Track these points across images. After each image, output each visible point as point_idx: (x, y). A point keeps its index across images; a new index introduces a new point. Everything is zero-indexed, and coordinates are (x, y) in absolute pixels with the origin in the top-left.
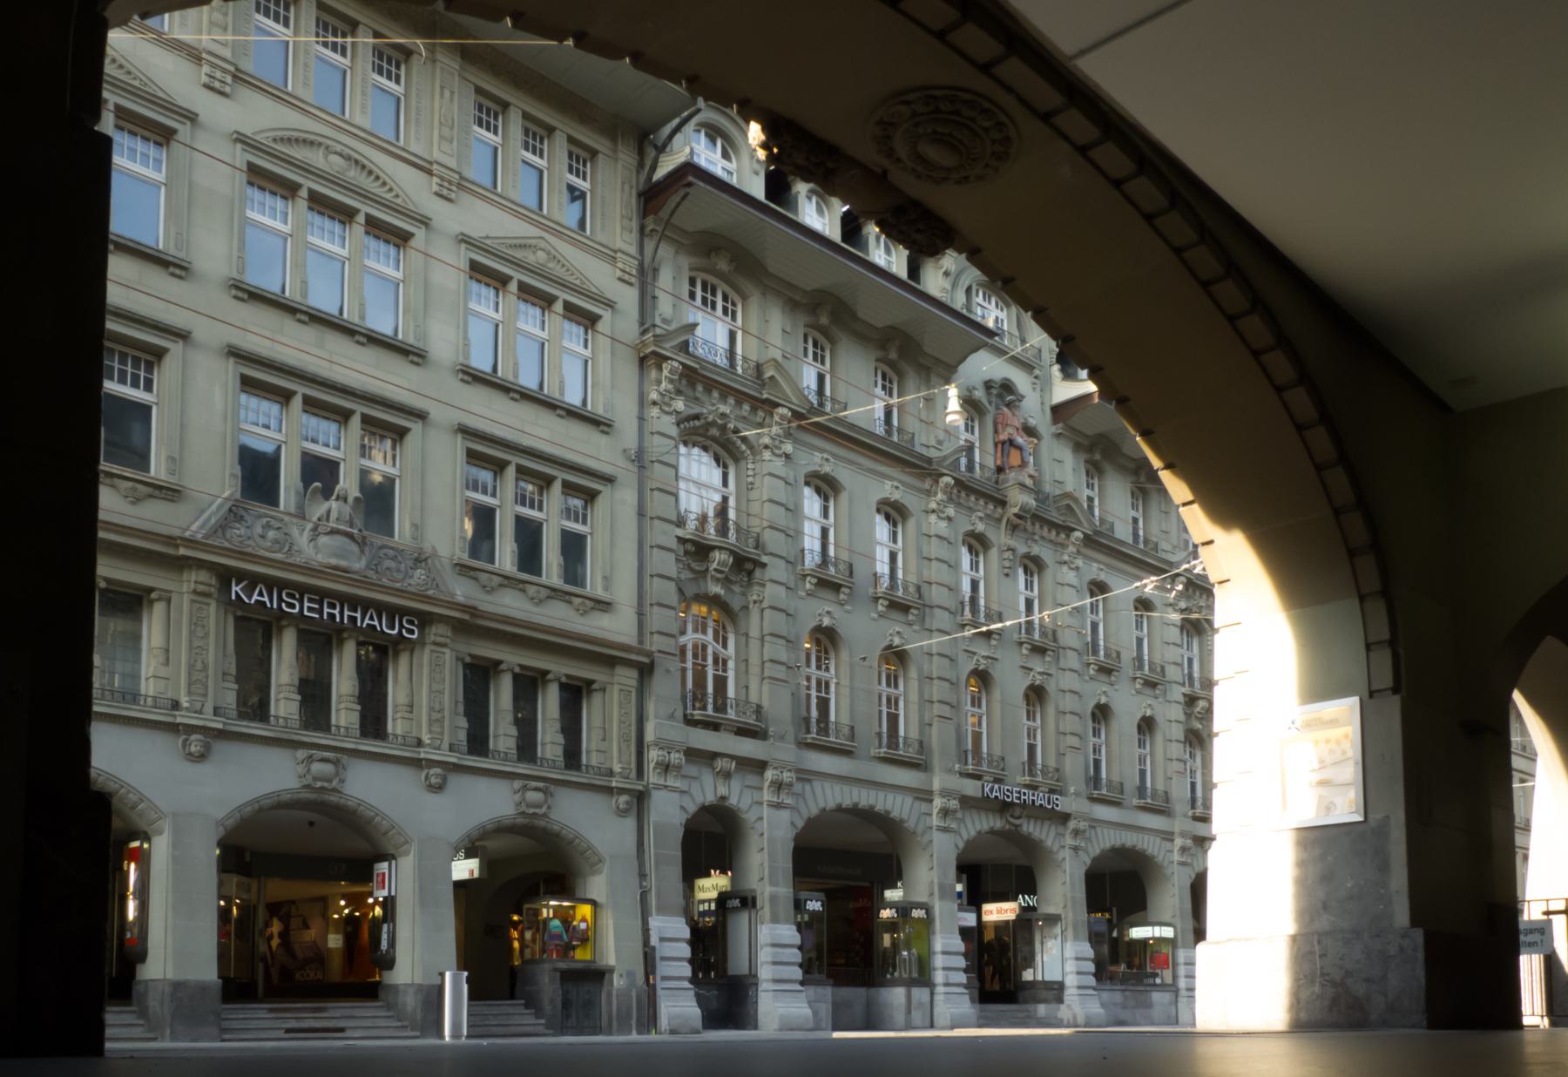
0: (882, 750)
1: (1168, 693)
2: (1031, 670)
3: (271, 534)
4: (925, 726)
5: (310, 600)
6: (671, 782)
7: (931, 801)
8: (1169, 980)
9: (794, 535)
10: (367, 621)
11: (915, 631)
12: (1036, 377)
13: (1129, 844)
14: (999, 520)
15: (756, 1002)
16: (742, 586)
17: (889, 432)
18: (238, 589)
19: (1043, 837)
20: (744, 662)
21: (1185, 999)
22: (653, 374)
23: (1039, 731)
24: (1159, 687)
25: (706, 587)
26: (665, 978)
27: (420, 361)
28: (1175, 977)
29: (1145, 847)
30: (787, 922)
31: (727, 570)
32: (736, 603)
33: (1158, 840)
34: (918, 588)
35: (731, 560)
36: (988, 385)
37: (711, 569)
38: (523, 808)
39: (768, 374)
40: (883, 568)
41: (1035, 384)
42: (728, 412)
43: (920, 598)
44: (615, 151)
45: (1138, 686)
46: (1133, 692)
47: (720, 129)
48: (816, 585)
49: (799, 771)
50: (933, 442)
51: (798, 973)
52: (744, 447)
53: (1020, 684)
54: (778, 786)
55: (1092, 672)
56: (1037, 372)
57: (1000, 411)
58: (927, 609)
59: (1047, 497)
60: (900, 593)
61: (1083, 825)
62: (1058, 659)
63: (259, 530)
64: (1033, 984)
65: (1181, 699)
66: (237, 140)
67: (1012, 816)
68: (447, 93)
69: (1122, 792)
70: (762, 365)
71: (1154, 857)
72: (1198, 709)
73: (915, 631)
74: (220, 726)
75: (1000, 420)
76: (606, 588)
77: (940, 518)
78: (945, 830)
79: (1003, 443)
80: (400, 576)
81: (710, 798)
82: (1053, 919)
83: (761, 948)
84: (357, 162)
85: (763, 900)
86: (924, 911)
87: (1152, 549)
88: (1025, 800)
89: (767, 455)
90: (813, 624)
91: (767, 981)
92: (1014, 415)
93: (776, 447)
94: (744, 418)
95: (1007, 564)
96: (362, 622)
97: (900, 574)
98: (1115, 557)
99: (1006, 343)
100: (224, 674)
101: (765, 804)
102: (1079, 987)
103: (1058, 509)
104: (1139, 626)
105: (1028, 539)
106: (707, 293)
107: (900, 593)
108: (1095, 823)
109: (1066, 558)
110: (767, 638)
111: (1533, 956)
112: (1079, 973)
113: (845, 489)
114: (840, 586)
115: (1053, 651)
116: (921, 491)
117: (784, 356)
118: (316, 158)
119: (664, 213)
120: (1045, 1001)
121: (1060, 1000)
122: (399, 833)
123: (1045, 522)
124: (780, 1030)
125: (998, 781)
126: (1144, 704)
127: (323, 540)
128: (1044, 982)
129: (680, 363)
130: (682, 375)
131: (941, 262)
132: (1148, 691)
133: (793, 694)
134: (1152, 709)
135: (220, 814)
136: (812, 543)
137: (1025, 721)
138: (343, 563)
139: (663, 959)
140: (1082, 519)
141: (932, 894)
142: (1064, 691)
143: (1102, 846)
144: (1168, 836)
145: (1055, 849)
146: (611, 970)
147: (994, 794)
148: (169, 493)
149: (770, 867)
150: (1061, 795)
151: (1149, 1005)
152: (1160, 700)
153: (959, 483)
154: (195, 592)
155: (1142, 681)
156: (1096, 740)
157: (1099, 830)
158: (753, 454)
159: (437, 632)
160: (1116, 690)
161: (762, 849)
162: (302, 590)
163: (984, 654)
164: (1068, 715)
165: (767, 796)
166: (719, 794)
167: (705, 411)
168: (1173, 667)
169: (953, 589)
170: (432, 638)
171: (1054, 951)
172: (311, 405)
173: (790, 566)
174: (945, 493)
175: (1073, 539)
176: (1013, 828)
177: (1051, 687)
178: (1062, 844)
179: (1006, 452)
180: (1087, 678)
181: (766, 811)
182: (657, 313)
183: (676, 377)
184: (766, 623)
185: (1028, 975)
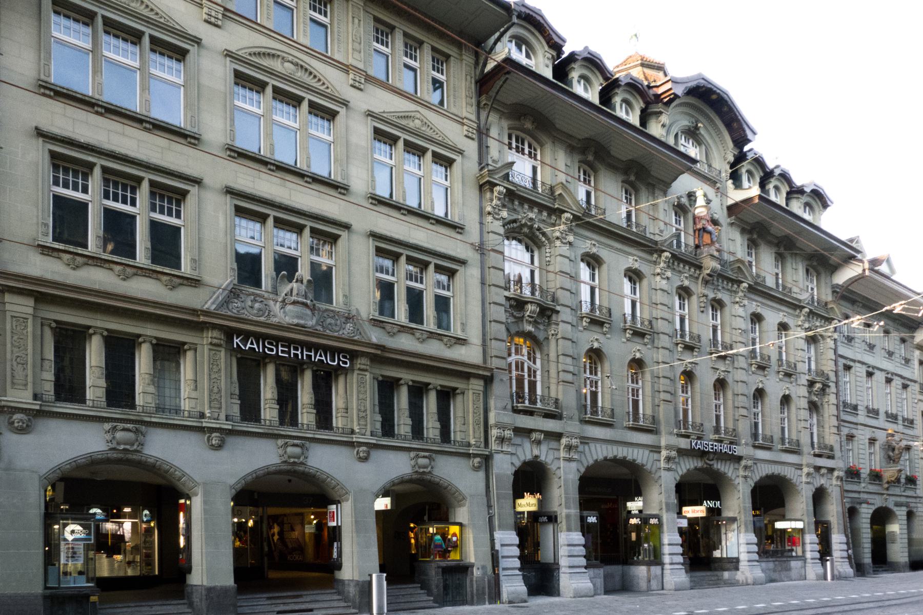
2: (718, 369)
3: (257, 305)
5: (282, 346)
10: (318, 357)
13: (776, 472)
14: (697, 278)
15: (559, 580)
18: (238, 341)
19: (726, 471)
21: (810, 565)
22: (488, 195)
26: (504, 569)
27: (196, 142)
28: (804, 551)
30: (576, 531)
32: (541, 336)
33: (647, 452)
38: (417, 469)
40: (628, 310)
43: (651, 328)
44: (461, 55)
48: (632, 334)
49: (582, 438)
50: (657, 231)
52: (544, 239)
54: (569, 448)
55: (753, 369)
56: (718, 185)
61: (750, 463)
62: (733, 362)
63: (250, 303)
66: (227, 55)
68: (356, 21)
69: (772, 442)
71: (791, 480)
72: (816, 389)
74: (374, 442)
76: (463, 330)
77: (740, 306)
78: (669, 470)
79: (699, 230)
80: (337, 329)
81: (529, 457)
84: (302, 67)
85: (562, 518)
86: (639, 519)
89: (828, 340)
91: (565, 567)
93: (496, 213)
94: (544, 220)
95: (703, 305)
96: (315, 358)
100: (231, 394)
102: (749, 561)
103: (732, 270)
108: (757, 461)
109: (738, 300)
113: (605, 263)
116: (650, 262)
118: (276, 65)
119: (492, 93)
121: (737, 569)
122: (342, 488)
124: (574, 597)
125: (699, 438)
127: (289, 308)
128: (727, 558)
129: (505, 187)
131: (660, 118)
132: (787, 379)
135: (232, 481)
136: (585, 295)
138: (302, 322)
139: (503, 557)
142: (737, 382)
143: (761, 475)
144: (799, 467)
146: (472, 566)
148: (194, 282)
151: (789, 569)
152: (649, 346)
154: (211, 344)
157: (758, 465)
159: (361, 362)
162: (277, 340)
165: (563, 454)
167: (520, 217)
169: (671, 322)
170: (358, 366)
172: (280, 223)
174: (665, 262)
177: (730, 380)
180: (750, 373)
181: (562, 464)
182: (489, 157)
184: (559, 348)
185: (717, 554)
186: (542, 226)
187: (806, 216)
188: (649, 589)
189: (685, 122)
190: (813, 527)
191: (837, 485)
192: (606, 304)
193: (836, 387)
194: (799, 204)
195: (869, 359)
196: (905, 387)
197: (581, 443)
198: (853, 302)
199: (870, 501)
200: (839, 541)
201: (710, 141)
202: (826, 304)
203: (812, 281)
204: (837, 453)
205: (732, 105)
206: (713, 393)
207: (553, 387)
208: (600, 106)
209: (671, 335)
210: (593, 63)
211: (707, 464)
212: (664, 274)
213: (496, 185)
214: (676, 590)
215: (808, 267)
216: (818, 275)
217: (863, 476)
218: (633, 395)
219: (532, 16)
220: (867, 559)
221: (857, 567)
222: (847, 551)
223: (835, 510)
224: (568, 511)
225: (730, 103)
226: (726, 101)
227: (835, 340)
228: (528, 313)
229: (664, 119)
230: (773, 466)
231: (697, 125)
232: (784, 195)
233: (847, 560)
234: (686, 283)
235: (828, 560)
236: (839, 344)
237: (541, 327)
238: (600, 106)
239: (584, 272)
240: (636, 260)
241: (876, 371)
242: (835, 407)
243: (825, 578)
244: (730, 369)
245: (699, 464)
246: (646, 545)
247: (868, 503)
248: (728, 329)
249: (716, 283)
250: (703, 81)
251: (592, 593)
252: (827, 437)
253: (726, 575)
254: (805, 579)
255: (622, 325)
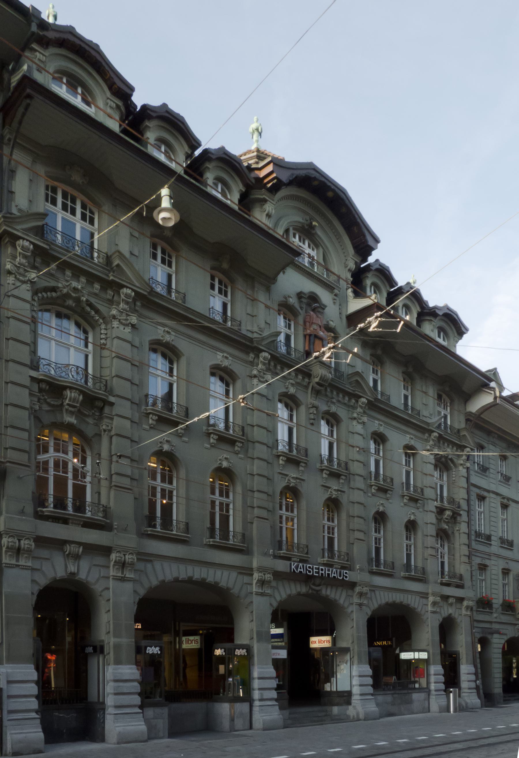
0: (325, 559)
1: (426, 505)
2: (329, 488)
4: (247, 523)
6: (22, 562)
7: (252, 575)
8: (424, 685)
9: (273, 432)
11: (240, 458)
12: (336, 295)
13: (398, 601)
14: (307, 387)
15: (104, 722)
16: (95, 419)
17: (225, 321)
19: (337, 598)
20: (96, 474)
21: (434, 697)
23: (413, 547)
24: (420, 501)
25: (63, 417)
26: (10, 712)
28: (428, 683)
29: (409, 602)
30: (129, 663)
31: (78, 405)
32: (89, 430)
33: (418, 598)
34: (243, 428)
35: (81, 398)
36: (300, 295)
37: (65, 404)
39: (116, 262)
40: (325, 451)
41: (335, 299)
42: (79, 287)
43: (243, 435)
45: (405, 501)
46: (402, 504)
47: (78, 78)
48: (217, 440)
49: (139, 554)
50: (255, 329)
51: (137, 700)
52: (452, 465)
53: (322, 496)
54: (122, 565)
55: (373, 491)
56: (336, 291)
57: (308, 314)
58: (250, 444)
59: (343, 375)
60: (231, 432)
61: (365, 590)
62: (424, 505)
64: (331, 692)
65: (434, 510)
67: (314, 584)
69: (393, 569)
70: (111, 256)
71: (415, 609)
72: (446, 516)
73: (240, 458)
75: (308, 320)
77: (358, 422)
78: (262, 594)
79: (310, 335)
81: (61, 573)
82: (345, 651)
83: (108, 683)
85: (109, 649)
86: (245, 651)
87: (417, 414)
88: (322, 574)
89: (461, 468)
90: (216, 465)
91: (111, 706)
92: (318, 317)
93: (261, 377)
94: (96, 294)
95: (312, 416)
97: (231, 419)
98: (387, 416)
99: (316, 270)
101: (111, 577)
102: (361, 695)
103: (351, 383)
104: (408, 463)
105: (328, 402)
106: (222, 285)
107: (231, 432)
108: (374, 588)
109: (355, 415)
110: (115, 458)
111: (415, 653)
112: (361, 685)
113: (183, 355)
114: (235, 441)
115: (346, 476)
116: (246, 362)
117: (132, 254)
119: (15, 124)
120: (337, 704)
121: (349, 703)
123: (340, 390)
124: (118, 743)
125: (302, 561)
126: (409, 513)
128: (337, 692)
129: (31, 242)
130: (134, 300)
131: (264, 207)
132: (412, 504)
133: (135, 498)
134: (415, 515)
136: (282, 434)
137: (373, 533)
139: (9, 697)
140: (366, 389)
141: (252, 638)
142: (353, 503)
143: (379, 603)
144: (425, 595)
145: (346, 605)
147: (299, 570)
149: (113, 623)
150: (350, 570)
151: (410, 702)
152: (421, 510)
153: (274, 358)
155: (408, 498)
156: (377, 535)
157: (377, 593)
158: (106, 323)
160: (390, 503)
161: (109, 611)
163: (335, 488)
164: (429, 537)
165: (112, 572)
166: (69, 571)
167: (60, 285)
168: (429, 489)
169: (366, 465)
171: (345, 672)
173: (135, 407)
174: (264, 364)
175: (360, 403)
176: (315, 592)
177: (344, 499)
178: (351, 602)
179: (312, 341)
180: (370, 495)
181: (111, 583)
182: (13, 205)
183: (267, 362)
184: (113, 447)
185: (327, 687)
186: (93, 300)
187: (440, 341)
188: (233, 729)
189: (298, 218)
190: (439, 657)
191: (466, 615)
192: (303, 444)
193: (468, 516)
194: (431, 327)
195: (504, 490)
196: (505, 507)
197: (370, 590)
198: (489, 433)
199: (502, 631)
200: (466, 672)
201: (328, 244)
202: (459, 431)
203: (445, 408)
204: (467, 582)
205: (349, 205)
206: (404, 533)
207: (104, 492)
208: (122, 135)
209: (270, 445)
210: (416, 296)
211: (313, 589)
212: (465, 465)
213: (19, 238)
214: (264, 729)
215: (441, 393)
216: (452, 401)
217: (495, 606)
218: (329, 533)
219: (451, 315)
220: (497, 687)
221: (485, 697)
222: (475, 681)
223: (464, 640)
224: (117, 640)
225: (347, 202)
226: (342, 200)
227: (468, 468)
228: (67, 401)
229: (269, 207)
230: (394, 594)
231: (311, 223)
232: (415, 315)
233: (475, 691)
234: (292, 390)
235: (451, 692)
236: (472, 472)
237: (90, 421)
238: (122, 135)
239: (282, 412)
240: (226, 358)
241: (511, 503)
242: (466, 536)
243: (448, 710)
244: (345, 489)
245: (304, 589)
246: (231, 679)
247: (500, 633)
248: (419, 475)
249: (329, 394)
250: (313, 172)
251: (146, 737)
252: (457, 566)
253: (336, 710)
254: (429, 712)
255: (205, 428)
